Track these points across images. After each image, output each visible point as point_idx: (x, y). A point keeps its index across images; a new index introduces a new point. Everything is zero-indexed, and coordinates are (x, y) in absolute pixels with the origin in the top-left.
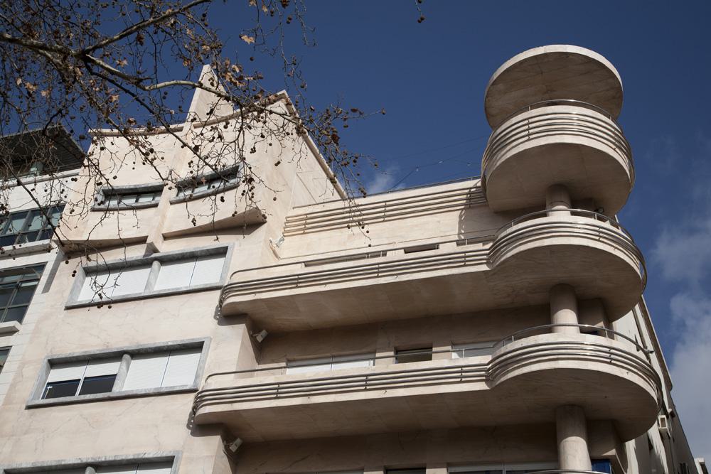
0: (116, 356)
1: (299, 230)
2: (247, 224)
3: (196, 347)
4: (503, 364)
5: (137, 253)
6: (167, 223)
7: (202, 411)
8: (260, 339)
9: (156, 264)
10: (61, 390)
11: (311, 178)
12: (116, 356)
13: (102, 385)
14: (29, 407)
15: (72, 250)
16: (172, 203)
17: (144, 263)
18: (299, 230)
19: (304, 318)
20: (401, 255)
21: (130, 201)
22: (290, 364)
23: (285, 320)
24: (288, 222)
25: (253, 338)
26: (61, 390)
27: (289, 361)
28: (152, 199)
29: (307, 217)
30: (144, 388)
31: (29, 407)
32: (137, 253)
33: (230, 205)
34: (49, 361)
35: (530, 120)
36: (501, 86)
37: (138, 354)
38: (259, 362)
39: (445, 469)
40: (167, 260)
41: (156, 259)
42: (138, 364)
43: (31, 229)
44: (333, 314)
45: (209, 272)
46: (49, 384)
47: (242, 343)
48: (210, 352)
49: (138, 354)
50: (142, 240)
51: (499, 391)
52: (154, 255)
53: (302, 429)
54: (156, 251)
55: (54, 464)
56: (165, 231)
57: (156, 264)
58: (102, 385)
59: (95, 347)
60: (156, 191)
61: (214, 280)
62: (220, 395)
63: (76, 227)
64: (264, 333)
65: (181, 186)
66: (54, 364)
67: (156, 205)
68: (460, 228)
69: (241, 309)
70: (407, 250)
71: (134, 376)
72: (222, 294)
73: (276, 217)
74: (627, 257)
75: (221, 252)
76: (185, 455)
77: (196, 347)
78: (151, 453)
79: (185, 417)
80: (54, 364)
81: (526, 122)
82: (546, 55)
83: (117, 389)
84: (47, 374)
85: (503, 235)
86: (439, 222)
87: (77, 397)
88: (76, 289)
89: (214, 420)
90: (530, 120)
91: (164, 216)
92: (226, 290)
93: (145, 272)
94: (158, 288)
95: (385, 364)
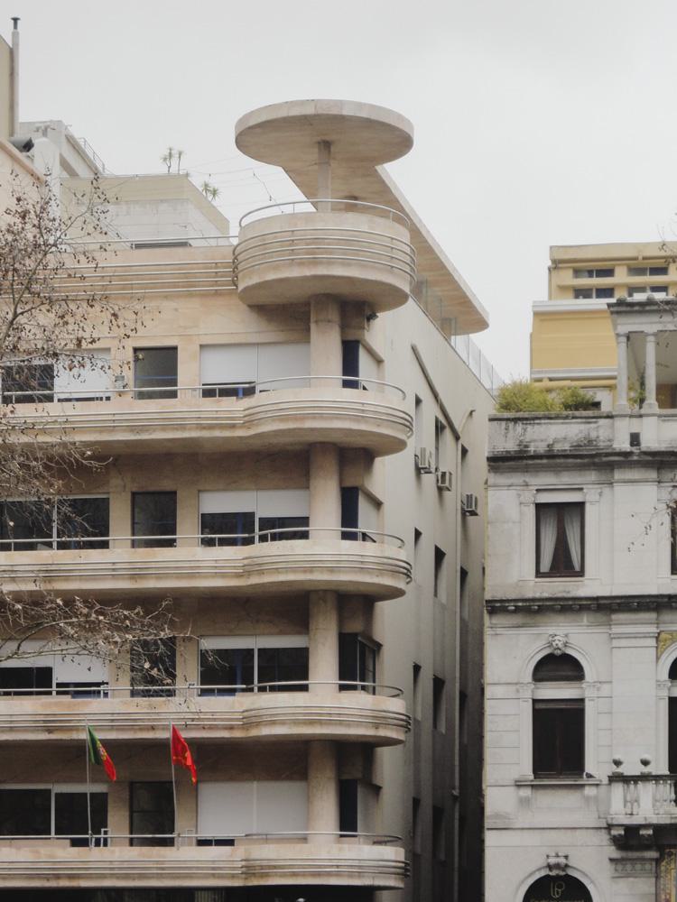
86: (176, 310)
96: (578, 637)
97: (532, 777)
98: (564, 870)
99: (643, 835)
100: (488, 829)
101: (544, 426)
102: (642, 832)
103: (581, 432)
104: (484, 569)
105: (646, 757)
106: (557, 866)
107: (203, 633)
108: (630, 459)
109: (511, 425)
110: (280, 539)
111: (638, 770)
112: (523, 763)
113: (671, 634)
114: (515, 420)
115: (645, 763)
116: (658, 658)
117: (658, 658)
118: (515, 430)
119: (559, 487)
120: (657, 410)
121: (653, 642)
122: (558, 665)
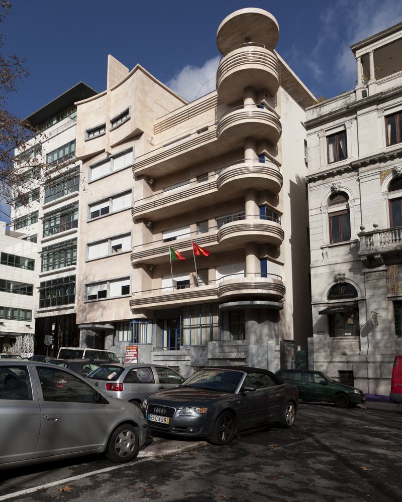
0: (107, 200)
1: (159, 131)
2: (137, 135)
3: (129, 192)
4: (221, 179)
5: (103, 157)
6: (111, 141)
7: (135, 215)
8: (151, 183)
9: (112, 159)
10: (95, 214)
11: (163, 100)
12: (107, 200)
13: (106, 211)
14: (88, 223)
15: (86, 159)
16: (111, 131)
17: (108, 160)
18: (159, 131)
19: (163, 172)
20: (197, 135)
21: (97, 134)
22: (165, 190)
23: (157, 173)
24: (155, 127)
25: (148, 183)
26: (95, 214)
27: (163, 189)
28: (98, 132)
29: (161, 123)
30: (16, 255)
31: (88, 223)
32: (103, 157)
33: (126, 130)
34: (89, 205)
35: (228, 60)
36: (221, 38)
37: (114, 197)
38: (154, 191)
39: (214, 220)
40: (115, 157)
41: (111, 157)
42: (115, 201)
43: (66, 154)
44: (172, 168)
45: (127, 160)
46: (92, 213)
47: (144, 186)
48: (135, 192)
49: (114, 197)
50: (103, 151)
51: (222, 190)
52: (110, 156)
53: (168, 215)
54: (110, 154)
55: (99, 240)
56: (111, 145)
57: (112, 159)
58: (106, 211)
59: (100, 198)
60: (103, 127)
61: (130, 163)
62: (139, 209)
63: (84, 148)
64: (152, 180)
65: (113, 122)
66: (91, 206)
67: (129, 119)
68: (216, 116)
69: (142, 173)
70: (198, 132)
71: (115, 205)
72: (133, 168)
73: (147, 130)
74: (269, 122)
75: (130, 150)
76: (134, 231)
77: (129, 192)
78: (124, 232)
79: (131, 218)
80: (91, 206)
81: (226, 62)
82: (234, 18)
83: (111, 211)
84: (90, 210)
85: (225, 118)
86: (208, 115)
87: (100, 216)
88: (90, 175)
89: (139, 218)
90: (228, 60)
91: (109, 138)
92: (133, 166)
93: (108, 164)
94: (115, 170)
95: (192, 185)
96: (345, 183)
97: (329, 244)
98: (343, 280)
99: (376, 258)
100: (368, 382)
101: (328, 106)
102: (376, 257)
103: (343, 102)
104: (306, 164)
105: (376, 223)
106: (340, 279)
107: (216, 216)
108: (338, 485)
109: (315, 110)
110: (194, 115)
111: (372, 229)
112: (326, 239)
113: (387, 171)
114: (316, 107)
115: (375, 226)
116: (381, 183)
117: (381, 183)
118: (316, 111)
119: (333, 127)
120: (375, 80)
121: (379, 176)
122: (338, 196)
